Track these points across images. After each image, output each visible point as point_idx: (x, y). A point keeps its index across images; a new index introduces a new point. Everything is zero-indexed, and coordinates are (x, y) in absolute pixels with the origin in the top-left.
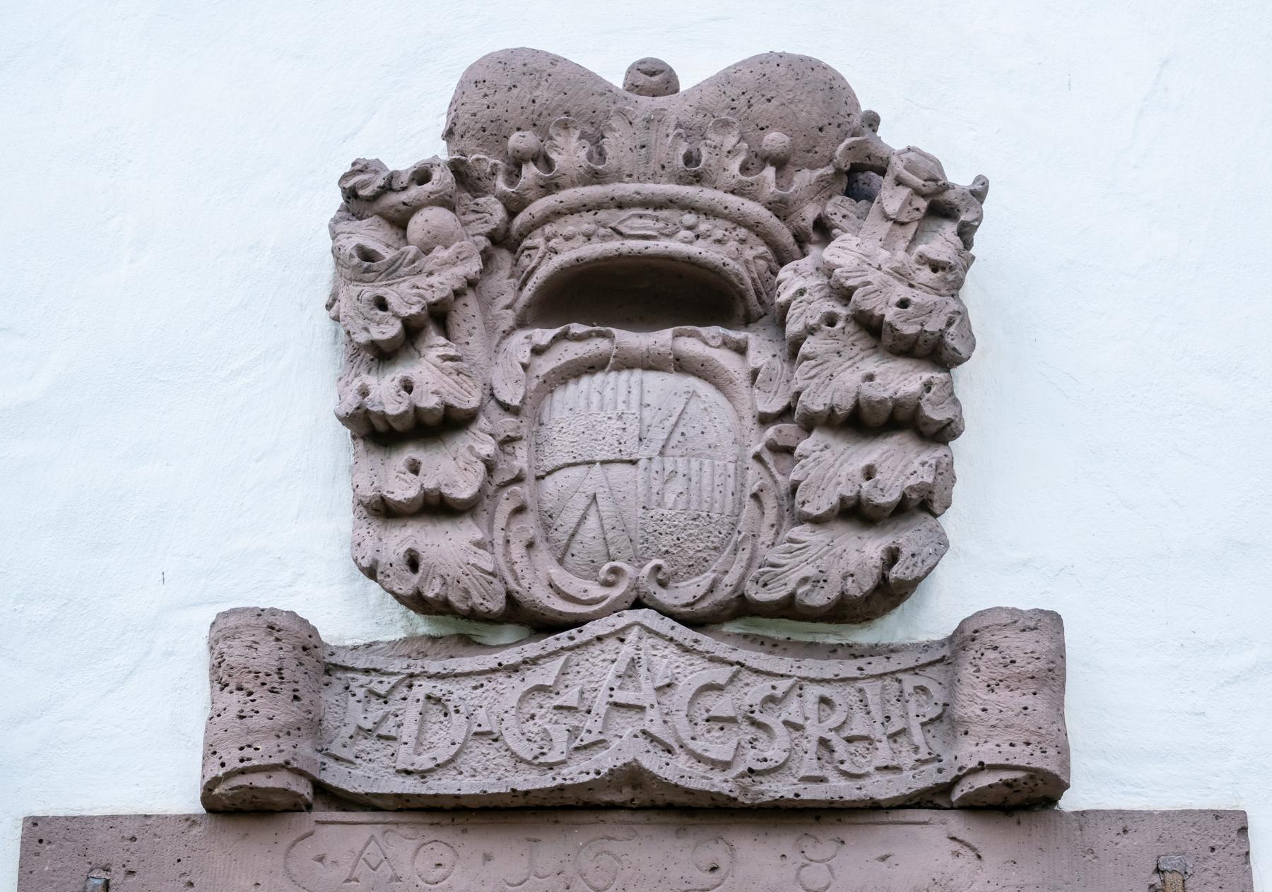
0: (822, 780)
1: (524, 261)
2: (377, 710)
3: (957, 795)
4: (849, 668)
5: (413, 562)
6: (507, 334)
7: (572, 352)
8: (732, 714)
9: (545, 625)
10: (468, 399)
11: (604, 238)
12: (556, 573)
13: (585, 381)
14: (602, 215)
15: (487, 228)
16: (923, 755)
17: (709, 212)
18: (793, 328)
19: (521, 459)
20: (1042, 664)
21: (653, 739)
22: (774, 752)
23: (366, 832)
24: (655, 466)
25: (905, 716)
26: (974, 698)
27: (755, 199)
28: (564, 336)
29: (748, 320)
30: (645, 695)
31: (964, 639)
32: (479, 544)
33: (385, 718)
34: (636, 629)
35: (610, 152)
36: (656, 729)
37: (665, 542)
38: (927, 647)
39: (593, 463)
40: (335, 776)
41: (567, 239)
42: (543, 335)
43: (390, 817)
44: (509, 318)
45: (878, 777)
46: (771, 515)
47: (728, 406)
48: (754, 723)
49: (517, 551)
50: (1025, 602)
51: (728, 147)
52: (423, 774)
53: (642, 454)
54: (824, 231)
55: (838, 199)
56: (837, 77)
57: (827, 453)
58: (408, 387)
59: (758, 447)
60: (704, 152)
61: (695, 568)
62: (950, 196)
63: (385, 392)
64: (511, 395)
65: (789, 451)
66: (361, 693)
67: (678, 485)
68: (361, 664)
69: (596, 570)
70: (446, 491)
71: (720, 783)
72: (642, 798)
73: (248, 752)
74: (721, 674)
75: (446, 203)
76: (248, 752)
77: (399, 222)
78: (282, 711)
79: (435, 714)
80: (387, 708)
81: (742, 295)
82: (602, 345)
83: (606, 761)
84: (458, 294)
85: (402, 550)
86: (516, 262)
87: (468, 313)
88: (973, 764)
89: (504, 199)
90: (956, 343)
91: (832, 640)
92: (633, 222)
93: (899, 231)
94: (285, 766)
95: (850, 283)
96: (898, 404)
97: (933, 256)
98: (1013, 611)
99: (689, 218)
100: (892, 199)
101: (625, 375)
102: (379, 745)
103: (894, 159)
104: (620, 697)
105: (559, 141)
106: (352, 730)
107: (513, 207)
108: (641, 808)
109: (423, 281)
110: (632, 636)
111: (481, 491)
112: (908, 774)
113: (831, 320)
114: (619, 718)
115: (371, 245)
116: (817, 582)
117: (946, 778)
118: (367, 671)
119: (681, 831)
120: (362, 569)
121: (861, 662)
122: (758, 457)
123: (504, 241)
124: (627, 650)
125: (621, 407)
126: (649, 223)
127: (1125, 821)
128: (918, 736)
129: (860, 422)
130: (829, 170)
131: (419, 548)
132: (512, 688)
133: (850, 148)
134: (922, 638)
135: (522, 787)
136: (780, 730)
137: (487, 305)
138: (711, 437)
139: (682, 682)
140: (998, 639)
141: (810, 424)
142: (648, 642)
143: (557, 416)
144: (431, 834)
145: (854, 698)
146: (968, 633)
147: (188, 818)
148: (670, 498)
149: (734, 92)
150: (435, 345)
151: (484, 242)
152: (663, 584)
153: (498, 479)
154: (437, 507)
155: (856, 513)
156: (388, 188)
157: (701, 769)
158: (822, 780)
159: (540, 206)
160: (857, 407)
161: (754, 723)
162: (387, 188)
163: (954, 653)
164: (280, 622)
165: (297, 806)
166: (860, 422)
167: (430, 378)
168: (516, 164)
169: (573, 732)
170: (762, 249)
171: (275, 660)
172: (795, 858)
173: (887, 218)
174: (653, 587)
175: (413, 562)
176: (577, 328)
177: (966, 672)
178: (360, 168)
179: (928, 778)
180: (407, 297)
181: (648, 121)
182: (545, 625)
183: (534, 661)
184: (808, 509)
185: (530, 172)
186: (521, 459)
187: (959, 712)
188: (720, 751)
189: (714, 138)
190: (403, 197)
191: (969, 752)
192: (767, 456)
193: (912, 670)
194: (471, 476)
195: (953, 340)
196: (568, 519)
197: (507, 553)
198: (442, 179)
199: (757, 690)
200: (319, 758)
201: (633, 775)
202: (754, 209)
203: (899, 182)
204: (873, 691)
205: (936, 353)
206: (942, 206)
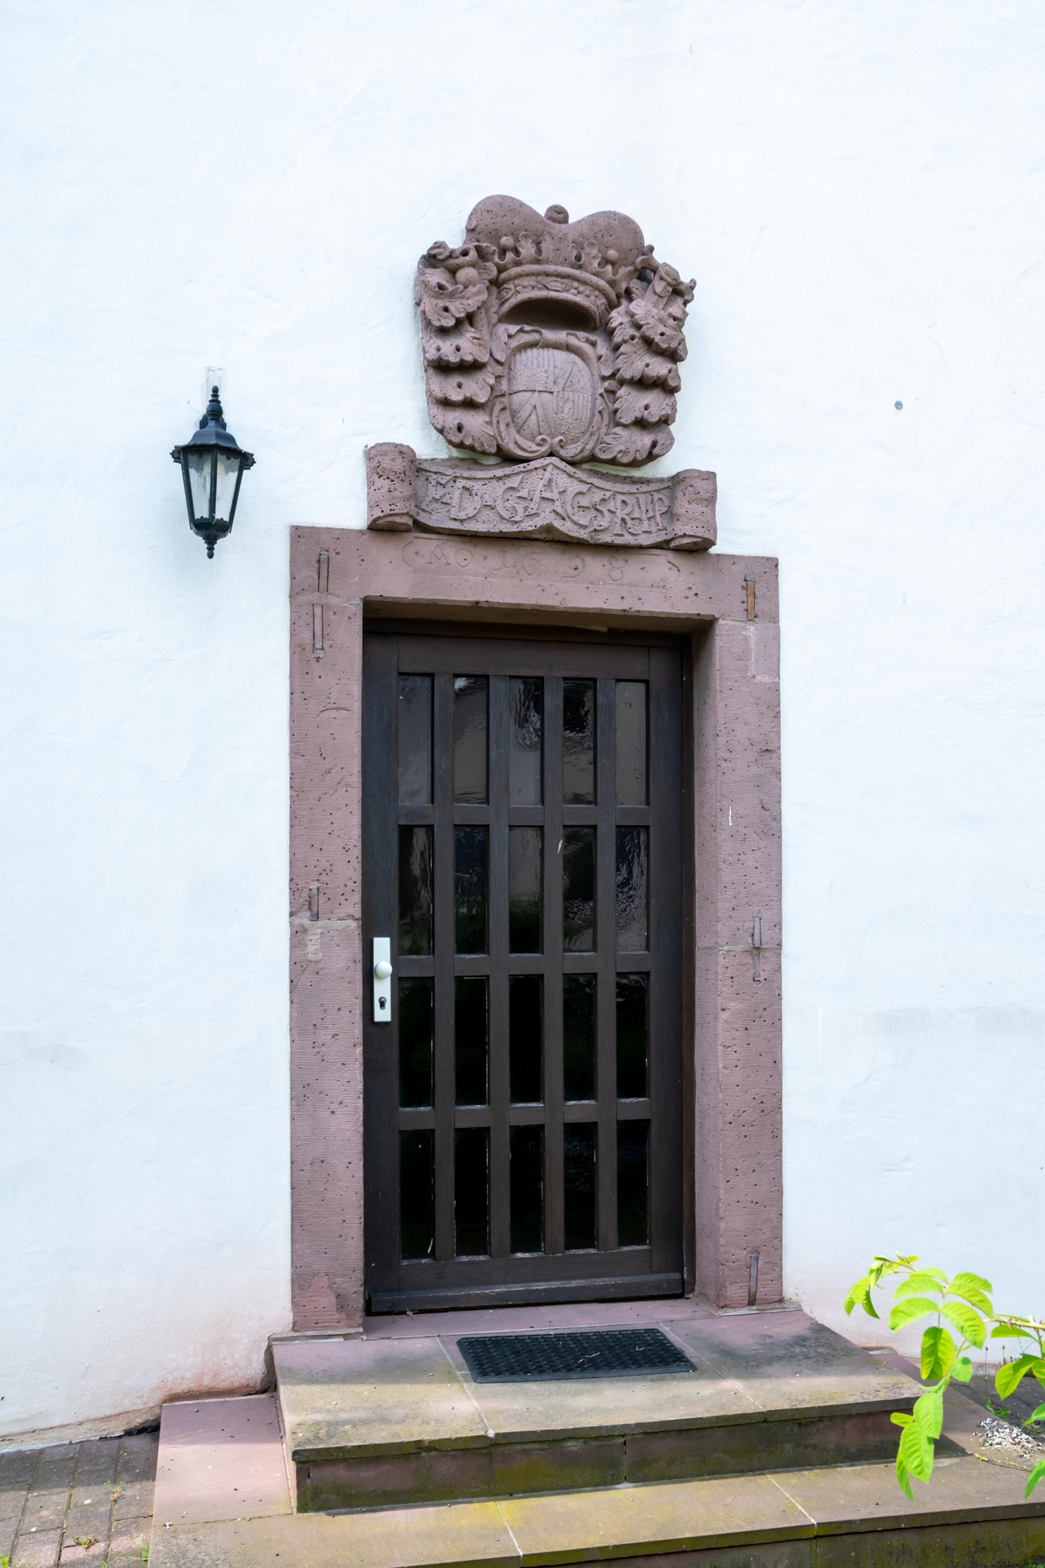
0: (622, 535)
1: (504, 293)
2: (441, 491)
3: (672, 545)
4: (633, 488)
5: (460, 428)
6: (495, 325)
7: (525, 338)
8: (588, 505)
9: (507, 458)
10: (484, 358)
11: (540, 289)
12: (518, 438)
13: (529, 352)
14: (539, 278)
15: (490, 277)
16: (660, 527)
17: (584, 282)
18: (617, 339)
19: (504, 386)
20: (709, 495)
21: (557, 514)
22: (605, 523)
23: (435, 543)
24: (561, 395)
25: (654, 510)
26: (683, 506)
27: (602, 278)
28: (521, 330)
29: (594, 329)
30: (555, 495)
31: (677, 481)
32: (487, 423)
33: (444, 495)
34: (551, 466)
35: (544, 251)
36: (559, 510)
37: (563, 429)
38: (662, 480)
39: (534, 391)
40: (423, 518)
41: (524, 287)
42: (513, 329)
43: (445, 537)
44: (495, 318)
45: (643, 535)
46: (606, 421)
47: (587, 368)
48: (596, 509)
49: (503, 427)
50: (704, 468)
51: (593, 254)
52: (462, 521)
53: (555, 389)
54: (628, 295)
55: (635, 280)
56: (637, 227)
57: (630, 397)
58: (458, 349)
59: (602, 391)
60: (583, 255)
61: (575, 440)
62: (682, 287)
63: (447, 349)
64: (500, 356)
65: (613, 392)
66: (434, 483)
67: (569, 405)
68: (433, 469)
69: (534, 438)
70: (475, 398)
71: (583, 534)
72: (549, 537)
73: (393, 507)
74: (584, 488)
75: (473, 265)
76: (393, 507)
77: (453, 272)
78: (402, 489)
79: (466, 495)
80: (445, 490)
81: (595, 320)
82: (535, 337)
83: (539, 522)
84: (479, 308)
85: (456, 422)
86: (499, 292)
87: (481, 319)
88: (681, 534)
89: (497, 265)
90: (682, 353)
91: (625, 474)
92: (554, 284)
93: (661, 300)
94: (407, 514)
95: (642, 323)
96: (658, 378)
97: (674, 314)
98: (699, 471)
99: (576, 284)
100: (659, 286)
101: (546, 351)
102: (442, 506)
103: (660, 269)
104: (545, 495)
105: (523, 243)
106: (430, 498)
107: (501, 270)
108: (552, 541)
109: (465, 302)
110: (550, 468)
111: (489, 400)
112: (654, 535)
113: (633, 338)
114: (544, 504)
115: (444, 282)
116: (625, 453)
117: (668, 537)
118: (436, 473)
119: (563, 552)
120: (436, 429)
121: (638, 486)
122: (601, 395)
123: (496, 284)
124: (547, 475)
125: (546, 367)
126: (559, 284)
127: (734, 559)
128: (658, 519)
129: (643, 383)
130: (630, 268)
131: (463, 422)
132: (499, 487)
133: (642, 261)
134: (659, 476)
135: (504, 530)
136: (607, 513)
137: (487, 311)
138: (582, 384)
139: (569, 490)
140: (693, 482)
141: (622, 382)
142: (556, 471)
143: (518, 367)
144: (462, 546)
145: (634, 501)
146: (681, 478)
147: (361, 531)
148: (566, 410)
149: (597, 230)
150: (470, 333)
151: (488, 284)
152: (562, 447)
153: (495, 394)
154: (469, 404)
155: (641, 424)
156: (451, 256)
157: (576, 527)
158: (622, 535)
159: (514, 271)
160: (642, 378)
161: (596, 509)
162: (450, 256)
163: (674, 485)
164: (404, 450)
165: (407, 530)
166: (643, 383)
167: (465, 346)
168: (503, 252)
169: (526, 509)
170: (604, 300)
171: (390, 465)
172: (607, 565)
173: (656, 293)
174: (558, 448)
175: (460, 428)
176: (527, 328)
177: (680, 494)
178: (438, 245)
179: (661, 537)
180: (458, 308)
181: (561, 238)
182: (507, 458)
183: (509, 476)
184: (623, 421)
185: (510, 256)
186: (504, 386)
187: (675, 511)
188: (583, 521)
189: (587, 250)
190: (456, 261)
191: (680, 528)
192: (605, 395)
193: (657, 491)
194: (484, 392)
195: (681, 353)
196: (523, 414)
197: (498, 427)
198: (473, 255)
199: (598, 496)
200: (416, 510)
201: (549, 528)
202: (602, 283)
203: (662, 278)
204: (642, 499)
205: (674, 356)
206: (680, 291)
